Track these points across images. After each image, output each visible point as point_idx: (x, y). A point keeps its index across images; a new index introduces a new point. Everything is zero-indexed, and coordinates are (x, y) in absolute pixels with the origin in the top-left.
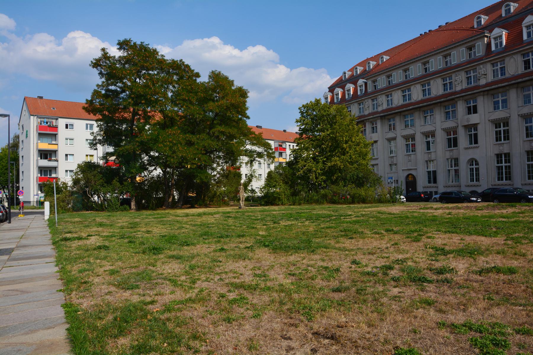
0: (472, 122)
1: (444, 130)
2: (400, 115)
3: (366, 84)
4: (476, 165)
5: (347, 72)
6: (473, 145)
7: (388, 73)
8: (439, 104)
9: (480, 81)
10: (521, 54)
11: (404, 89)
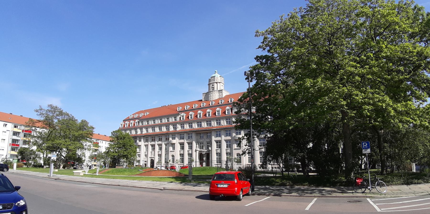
0: (173, 142)
1: (179, 143)
2: (214, 131)
4: (239, 156)
5: (132, 115)
11: (208, 120)
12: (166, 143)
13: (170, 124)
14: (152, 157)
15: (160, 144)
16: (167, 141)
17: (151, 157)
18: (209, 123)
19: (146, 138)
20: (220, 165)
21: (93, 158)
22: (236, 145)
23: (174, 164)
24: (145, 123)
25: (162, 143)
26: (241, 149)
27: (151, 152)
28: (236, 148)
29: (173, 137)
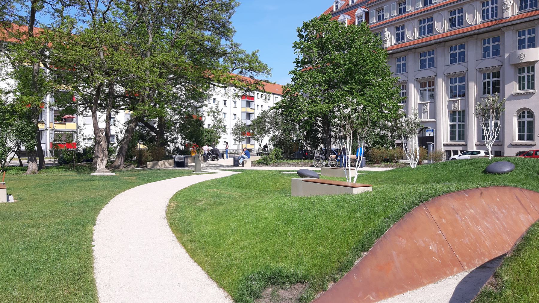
1: (479, 70)
3: (367, 14)
4: (528, 117)
6: (526, 91)
15: (456, 74)
19: (398, 60)
20: (463, 145)
21: (243, 134)
23: (531, 145)
26: (533, 93)
29: (399, 63)
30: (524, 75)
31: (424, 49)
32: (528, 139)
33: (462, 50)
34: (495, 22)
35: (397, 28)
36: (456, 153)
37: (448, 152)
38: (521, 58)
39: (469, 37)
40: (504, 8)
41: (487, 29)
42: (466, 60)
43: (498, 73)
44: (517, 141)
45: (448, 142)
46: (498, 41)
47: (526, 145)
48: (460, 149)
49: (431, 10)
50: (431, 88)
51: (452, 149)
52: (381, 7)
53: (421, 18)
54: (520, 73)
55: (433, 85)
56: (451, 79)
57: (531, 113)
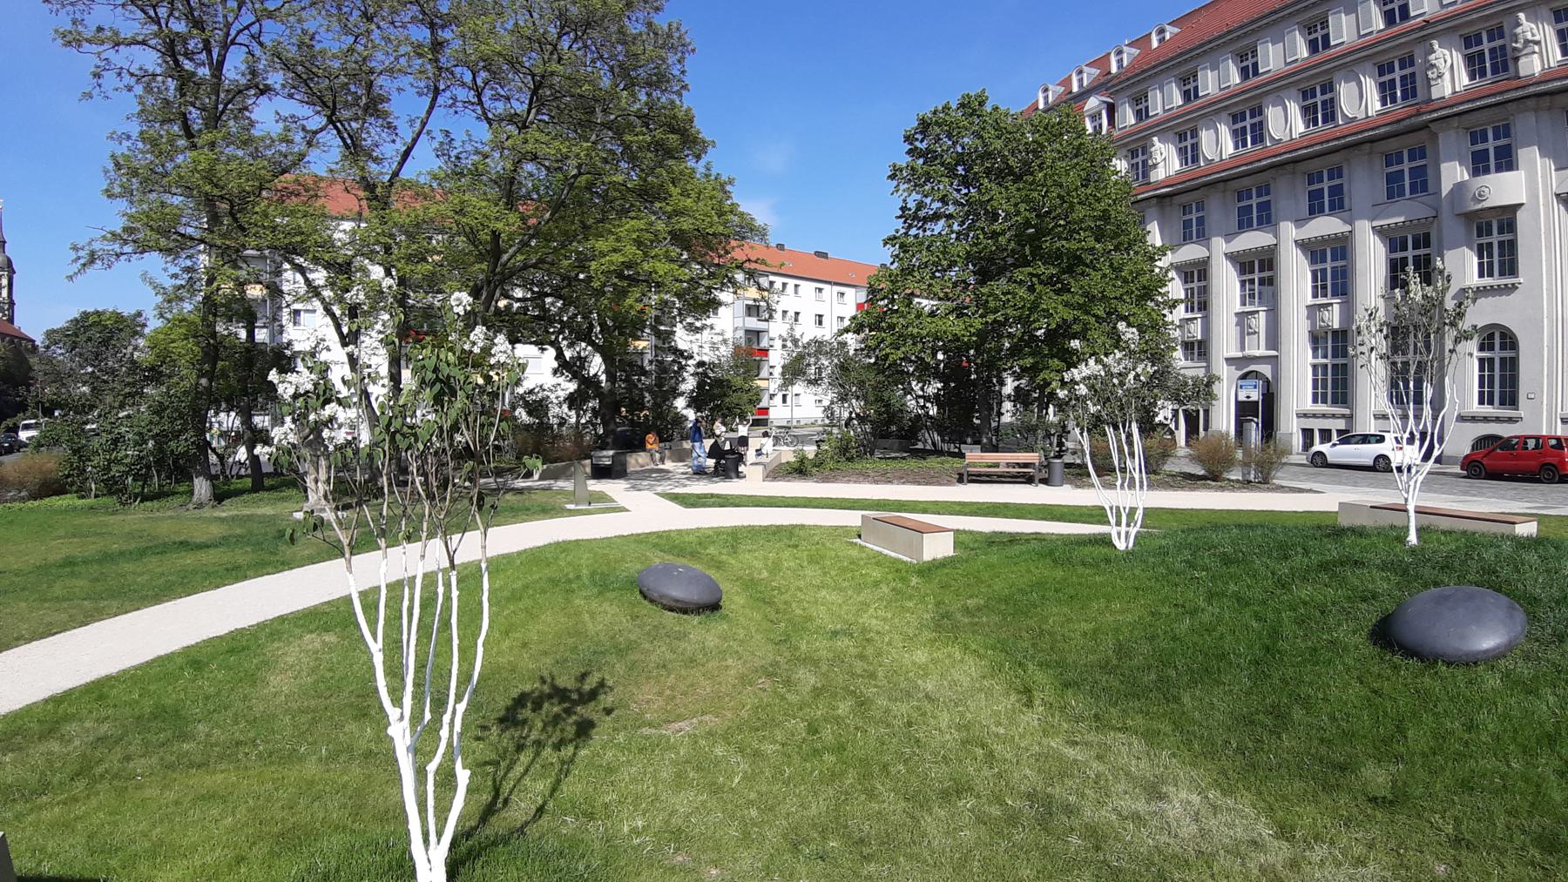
4: (1503, 347)
7: (1184, 69)
8: (1289, 168)
9: (1522, 61)
10: (1461, 36)
12: (1402, 219)
13: (1153, 135)
14: (1257, 353)
15: (1324, 240)
16: (1402, 204)
17: (1240, 354)
18: (1492, 51)
19: (1186, 209)
20: (1343, 416)
22: (1475, 260)
24: (1167, 99)
25: (1347, 228)
26: (1514, 287)
27: (1242, 316)
28: (1473, 279)
29: (1187, 217)
30: (1490, 241)
31: (1246, 182)
32: (1502, 403)
33: (1337, 182)
34: (1412, 110)
35: (1180, 135)
36: (1326, 435)
37: (1308, 434)
38: (1479, 198)
39: (1351, 149)
40: (1430, 76)
41: (1395, 127)
42: (1346, 206)
43: (1427, 236)
44: (1475, 407)
45: (1309, 408)
46: (1423, 156)
47: (1498, 420)
48: (1341, 424)
49: (1257, 88)
50: (1266, 274)
51: (1316, 425)
52: (1142, 91)
53: (1235, 110)
54: (1480, 235)
55: (1271, 268)
56: (1314, 250)
57: (1510, 338)
